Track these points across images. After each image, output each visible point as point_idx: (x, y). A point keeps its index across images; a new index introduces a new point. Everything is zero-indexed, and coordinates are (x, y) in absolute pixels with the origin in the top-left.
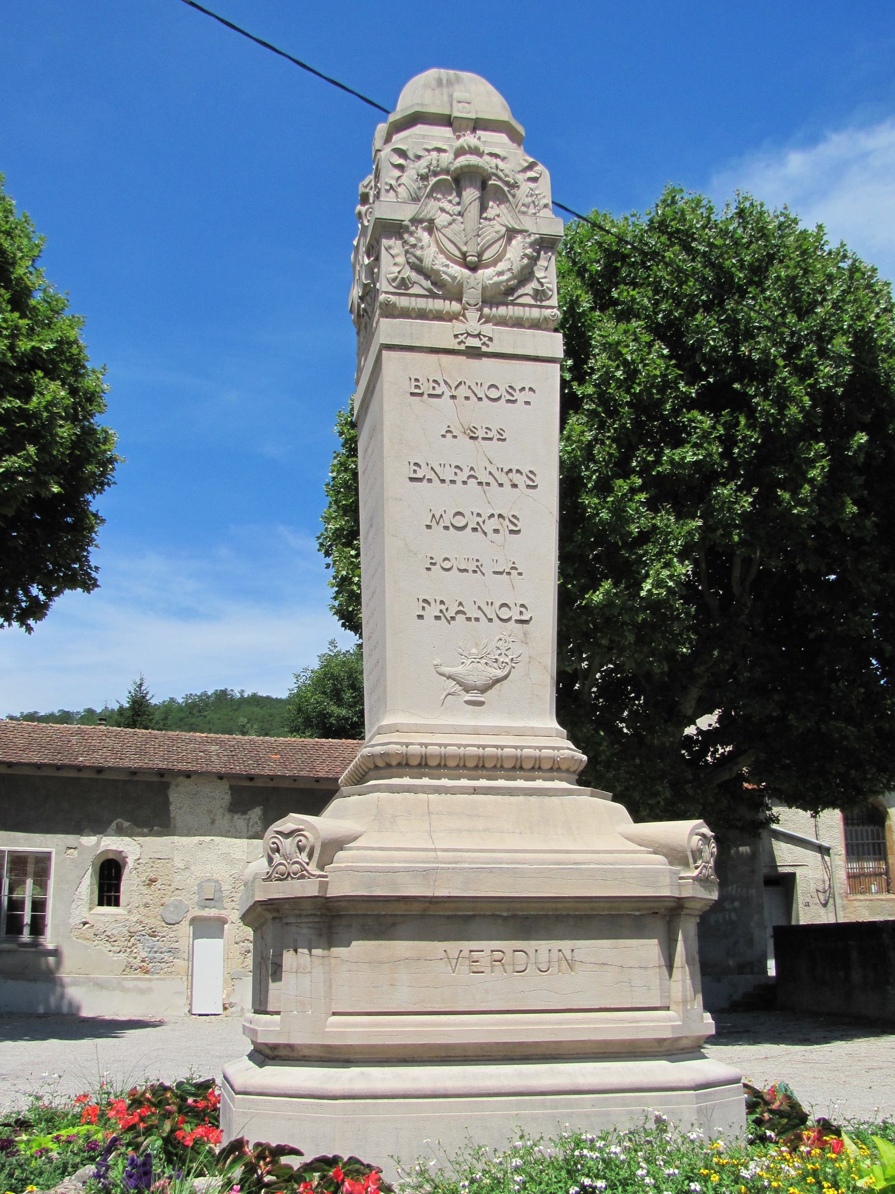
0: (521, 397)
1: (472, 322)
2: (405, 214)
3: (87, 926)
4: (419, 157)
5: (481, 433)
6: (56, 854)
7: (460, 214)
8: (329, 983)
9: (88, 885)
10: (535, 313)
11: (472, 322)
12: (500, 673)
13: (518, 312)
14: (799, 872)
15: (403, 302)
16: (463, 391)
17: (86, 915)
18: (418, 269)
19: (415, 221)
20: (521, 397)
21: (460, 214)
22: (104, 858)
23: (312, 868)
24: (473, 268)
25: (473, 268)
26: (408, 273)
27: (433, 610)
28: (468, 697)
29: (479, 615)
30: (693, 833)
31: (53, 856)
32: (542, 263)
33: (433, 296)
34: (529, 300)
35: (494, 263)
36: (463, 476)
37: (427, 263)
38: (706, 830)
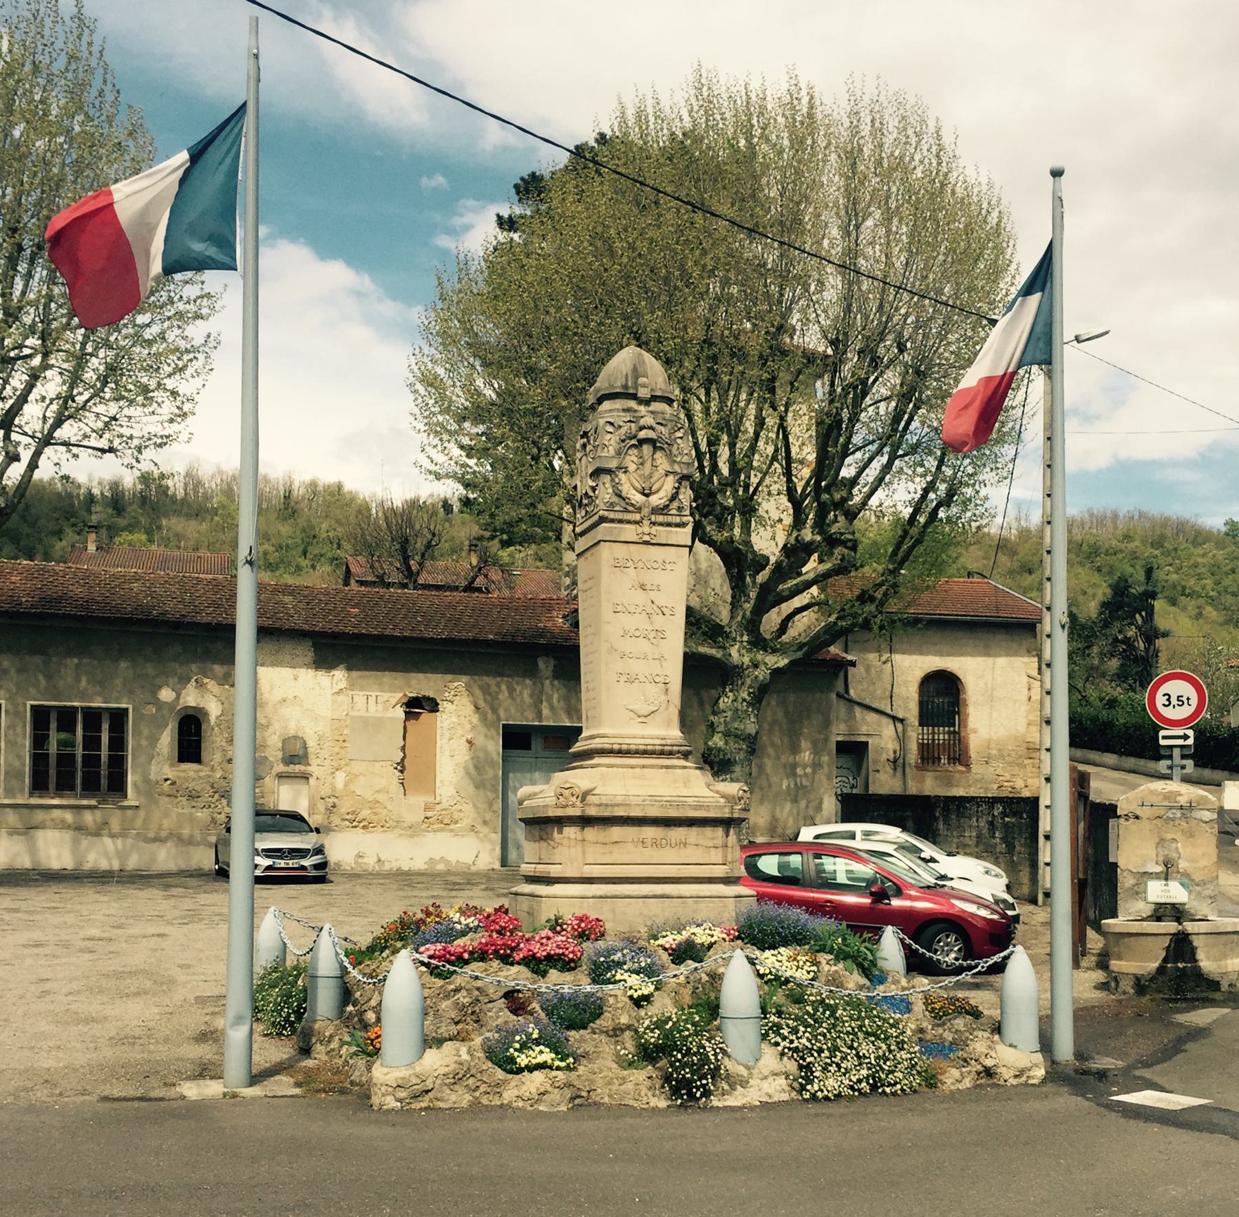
0: (668, 567)
1: (646, 529)
2: (613, 464)
3: (169, 782)
4: (620, 427)
5: (648, 587)
6: (133, 710)
7: (642, 464)
8: (584, 853)
9: (167, 739)
10: (678, 520)
11: (646, 529)
12: (655, 709)
13: (670, 519)
14: (870, 741)
15: (612, 515)
16: (640, 565)
17: (169, 772)
18: (619, 495)
19: (619, 468)
20: (668, 567)
21: (642, 464)
22: (183, 714)
23: (578, 803)
24: (647, 495)
25: (647, 495)
26: (615, 499)
27: (623, 678)
28: (640, 720)
29: (645, 680)
30: (740, 789)
31: (131, 711)
32: (682, 490)
33: (626, 511)
34: (674, 512)
35: (656, 492)
36: (639, 610)
37: (624, 494)
38: (746, 788)
